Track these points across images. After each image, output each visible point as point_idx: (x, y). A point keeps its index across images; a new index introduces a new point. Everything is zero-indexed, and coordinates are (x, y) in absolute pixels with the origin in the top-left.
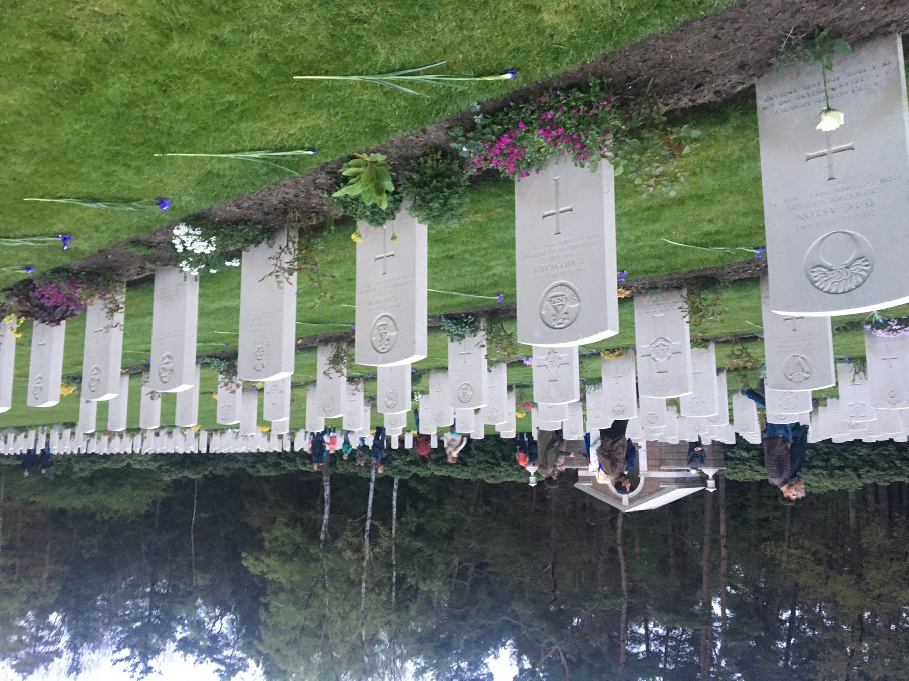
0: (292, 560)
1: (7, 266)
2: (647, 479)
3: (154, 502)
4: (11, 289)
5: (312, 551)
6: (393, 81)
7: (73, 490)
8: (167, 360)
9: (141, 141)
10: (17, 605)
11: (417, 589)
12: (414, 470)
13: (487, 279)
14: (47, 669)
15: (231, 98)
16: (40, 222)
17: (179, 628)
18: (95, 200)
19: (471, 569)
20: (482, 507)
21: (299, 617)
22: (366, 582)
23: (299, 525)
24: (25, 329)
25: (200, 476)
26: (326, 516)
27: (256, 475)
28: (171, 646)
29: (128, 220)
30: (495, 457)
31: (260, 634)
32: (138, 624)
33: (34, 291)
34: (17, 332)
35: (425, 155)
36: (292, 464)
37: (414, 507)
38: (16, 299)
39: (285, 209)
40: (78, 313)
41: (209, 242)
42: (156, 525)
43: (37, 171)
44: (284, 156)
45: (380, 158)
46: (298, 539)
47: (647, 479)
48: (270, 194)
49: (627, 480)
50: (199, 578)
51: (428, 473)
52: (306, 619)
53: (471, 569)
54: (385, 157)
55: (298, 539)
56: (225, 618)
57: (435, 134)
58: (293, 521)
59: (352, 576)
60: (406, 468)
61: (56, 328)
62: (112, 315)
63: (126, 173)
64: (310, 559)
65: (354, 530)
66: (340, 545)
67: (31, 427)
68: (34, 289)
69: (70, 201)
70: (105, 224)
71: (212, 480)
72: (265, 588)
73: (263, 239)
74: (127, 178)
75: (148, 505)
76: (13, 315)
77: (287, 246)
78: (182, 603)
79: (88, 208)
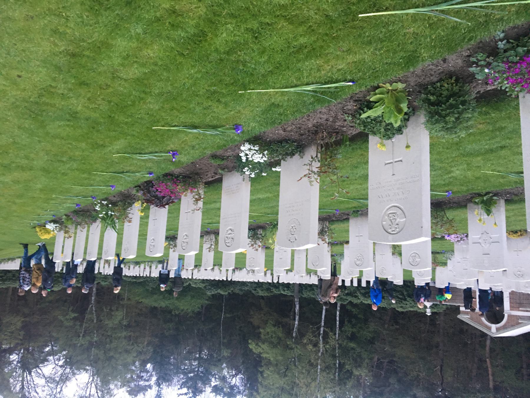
0: (277, 347)
1: (139, 172)
2: (510, 316)
3: (202, 306)
4: (140, 187)
5: (288, 343)
6: (442, 11)
7: (161, 297)
8: (230, 232)
9: (232, 81)
10: (132, 358)
11: (352, 373)
12: (350, 299)
13: (444, 180)
14: (144, 394)
15: (302, 40)
16: (161, 144)
17: (213, 380)
18: (195, 127)
19: (385, 364)
20: (392, 325)
21: (281, 382)
22: (320, 365)
23: (280, 326)
24: (146, 210)
25: (226, 293)
26: (297, 323)
27: (257, 294)
28: (208, 389)
29: (212, 140)
30: (403, 294)
31: (258, 388)
32: (192, 375)
33: (152, 187)
34: (142, 212)
35: (441, 80)
36: (277, 290)
37: (350, 322)
38: (142, 192)
39: (316, 131)
40: (176, 201)
41: (264, 155)
42: (203, 319)
43: (162, 107)
44: (329, 88)
45: (400, 86)
46: (280, 335)
47: (510, 316)
48: (309, 120)
49: (496, 317)
50: (225, 352)
51: (359, 301)
52: (284, 383)
53: (385, 364)
54: (404, 85)
55: (280, 335)
56: (238, 376)
57: (455, 61)
58: (278, 324)
59: (312, 361)
60: (345, 297)
61: (163, 210)
62: (197, 203)
63: (218, 107)
64: (287, 347)
65: (313, 332)
66: (305, 341)
67: (142, 262)
68: (153, 186)
69: (181, 128)
70: (199, 144)
71: (233, 296)
72: (261, 362)
73: (297, 152)
74: (219, 111)
75: (199, 308)
76: (140, 201)
77: (317, 156)
78: (215, 365)
79: (190, 133)
